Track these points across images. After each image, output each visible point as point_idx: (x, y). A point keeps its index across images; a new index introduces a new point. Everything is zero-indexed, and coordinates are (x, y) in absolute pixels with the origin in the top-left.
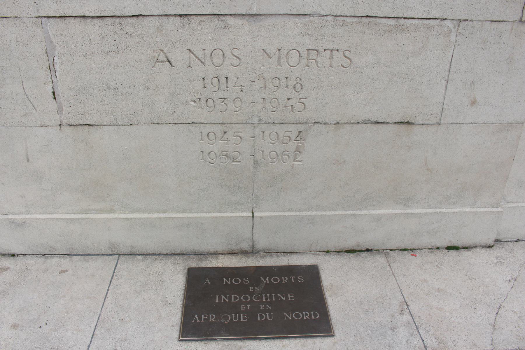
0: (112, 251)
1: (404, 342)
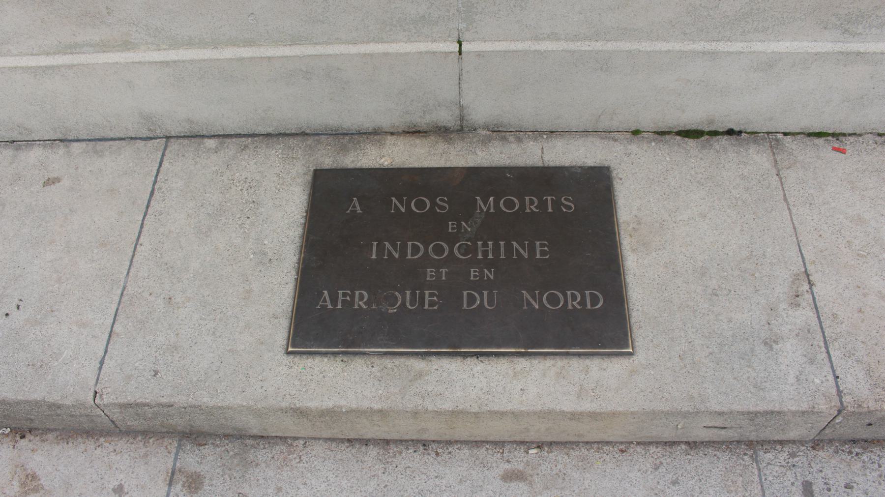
0: (150, 130)
1: (791, 379)
